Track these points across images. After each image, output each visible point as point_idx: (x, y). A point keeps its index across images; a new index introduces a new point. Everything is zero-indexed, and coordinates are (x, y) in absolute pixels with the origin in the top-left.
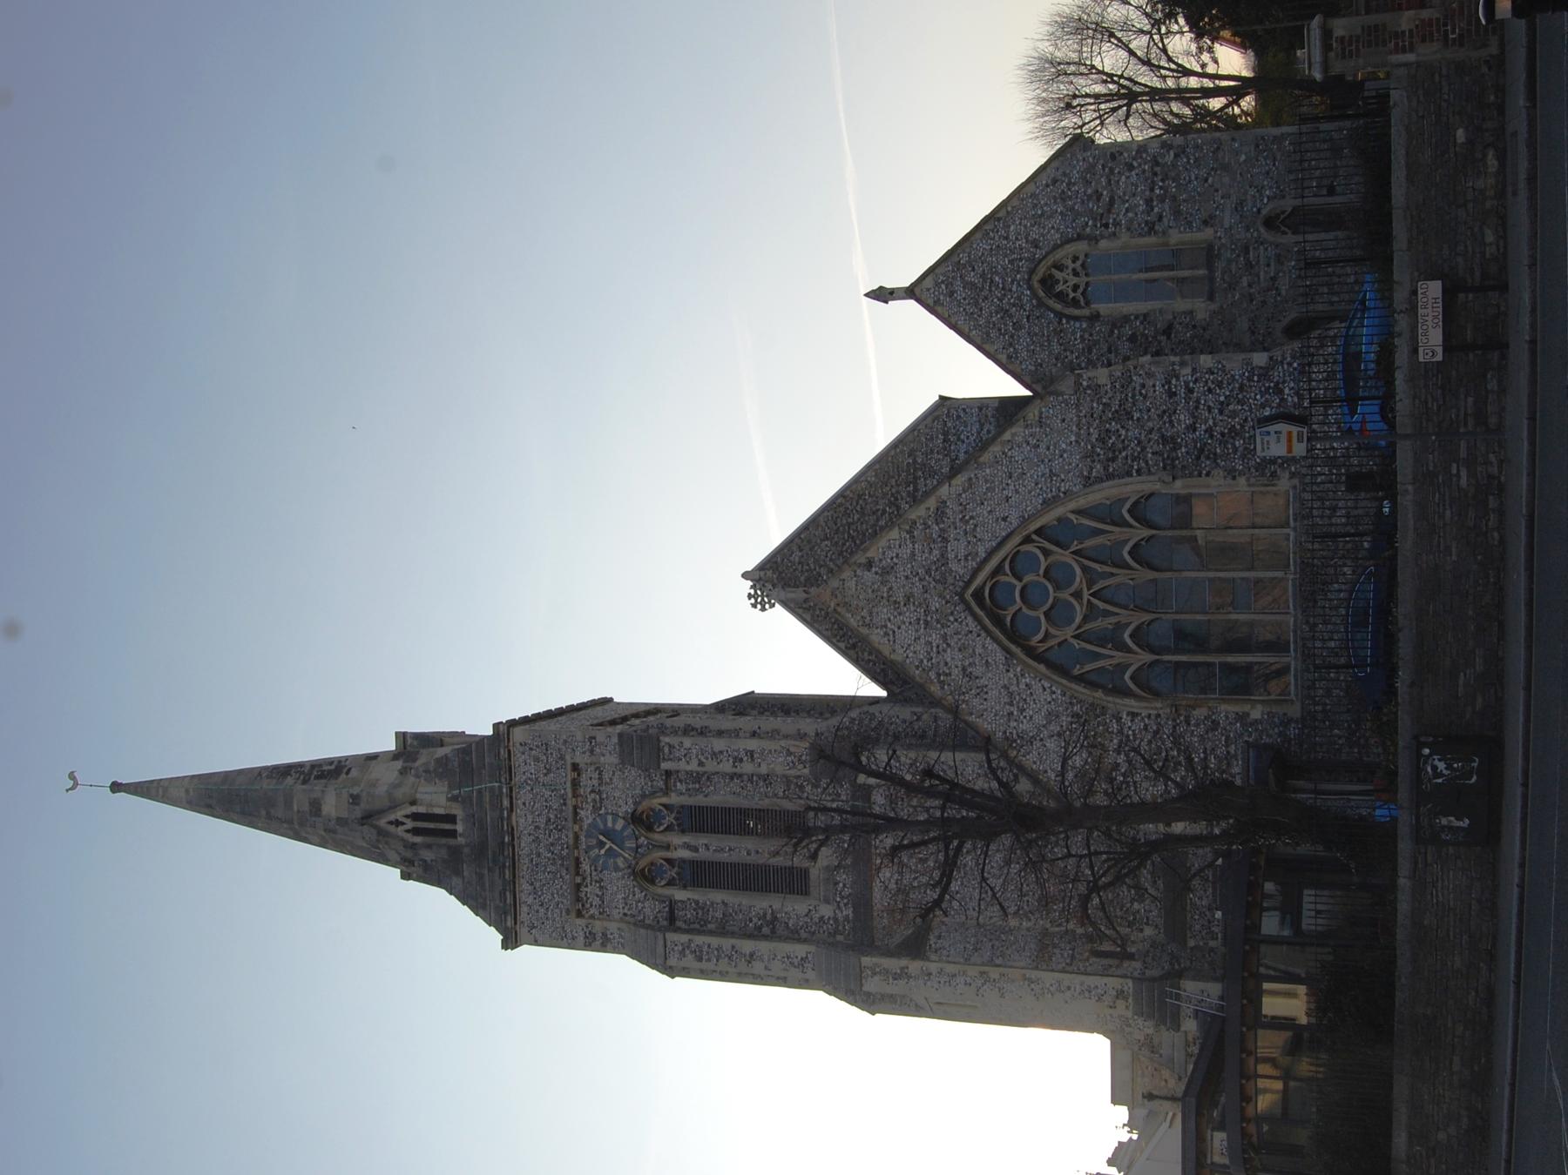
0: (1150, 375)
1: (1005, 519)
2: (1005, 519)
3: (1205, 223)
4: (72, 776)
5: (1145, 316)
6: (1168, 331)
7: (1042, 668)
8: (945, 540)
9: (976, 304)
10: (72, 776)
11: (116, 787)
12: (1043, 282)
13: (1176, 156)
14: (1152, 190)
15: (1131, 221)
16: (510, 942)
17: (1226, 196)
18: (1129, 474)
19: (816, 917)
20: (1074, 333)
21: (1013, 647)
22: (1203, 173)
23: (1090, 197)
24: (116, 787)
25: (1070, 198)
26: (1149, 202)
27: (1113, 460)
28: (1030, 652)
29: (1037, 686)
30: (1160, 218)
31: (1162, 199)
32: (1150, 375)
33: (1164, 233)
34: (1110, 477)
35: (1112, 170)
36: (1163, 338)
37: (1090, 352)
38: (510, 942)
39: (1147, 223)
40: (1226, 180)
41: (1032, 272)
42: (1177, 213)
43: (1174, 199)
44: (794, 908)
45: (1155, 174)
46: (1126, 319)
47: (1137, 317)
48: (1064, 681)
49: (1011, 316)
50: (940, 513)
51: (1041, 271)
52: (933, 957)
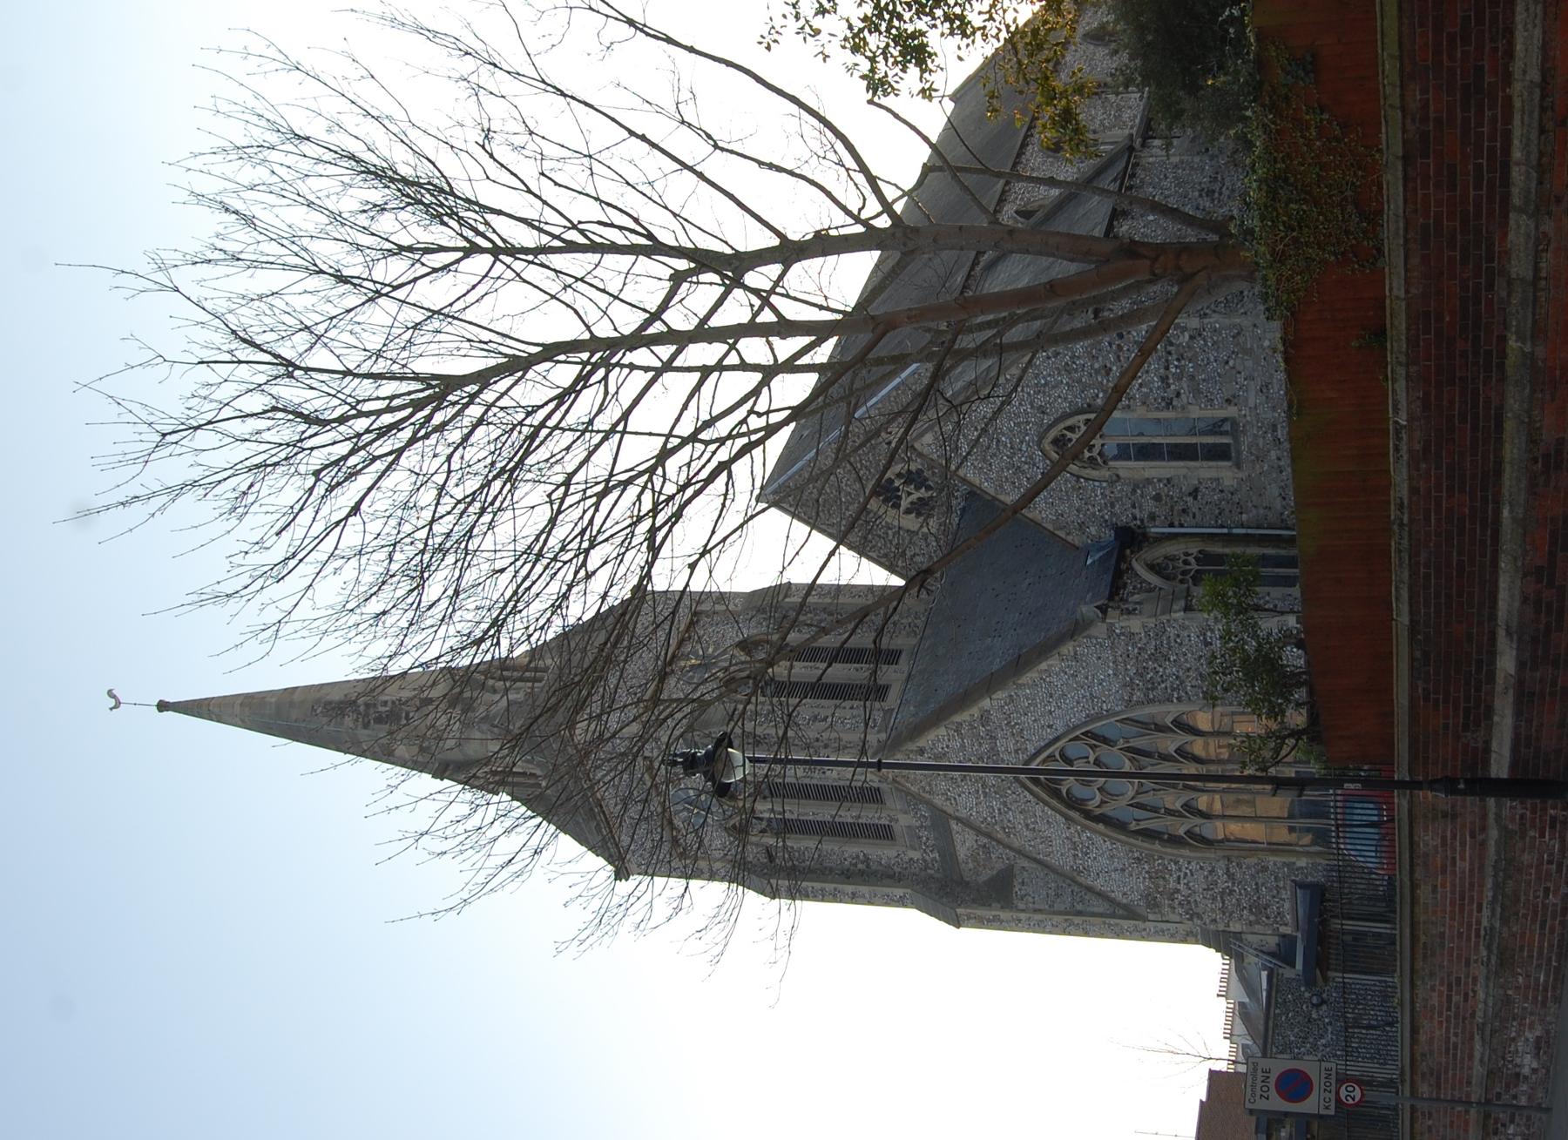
0: (1184, 628)
1: (1050, 726)
2: (1050, 726)
3: (1228, 401)
4: (111, 694)
5: (1169, 480)
6: (1194, 493)
7: (1101, 827)
8: (993, 738)
9: (984, 460)
10: (111, 694)
11: (163, 706)
12: (1055, 442)
13: (1191, 337)
14: (1167, 368)
15: (1146, 395)
16: (621, 874)
17: (1250, 378)
18: (1170, 700)
19: (906, 859)
20: (1093, 490)
21: (1071, 813)
22: (1223, 355)
23: (1097, 372)
24: (163, 706)
25: (1076, 371)
26: (1164, 379)
27: (1153, 689)
28: (1088, 815)
29: (1098, 839)
30: (1178, 394)
31: (1179, 378)
32: (1184, 628)
33: (1183, 408)
34: (1151, 701)
35: (1120, 348)
36: (1190, 499)
37: (1113, 505)
38: (621, 874)
39: (1163, 399)
40: (1249, 363)
41: (1041, 438)
42: (1196, 392)
43: (1192, 377)
44: (883, 853)
45: (1169, 353)
46: (1149, 481)
47: (1160, 480)
48: (1123, 838)
49: (1023, 472)
50: (985, 718)
51: (1053, 434)
52: (1021, 906)
